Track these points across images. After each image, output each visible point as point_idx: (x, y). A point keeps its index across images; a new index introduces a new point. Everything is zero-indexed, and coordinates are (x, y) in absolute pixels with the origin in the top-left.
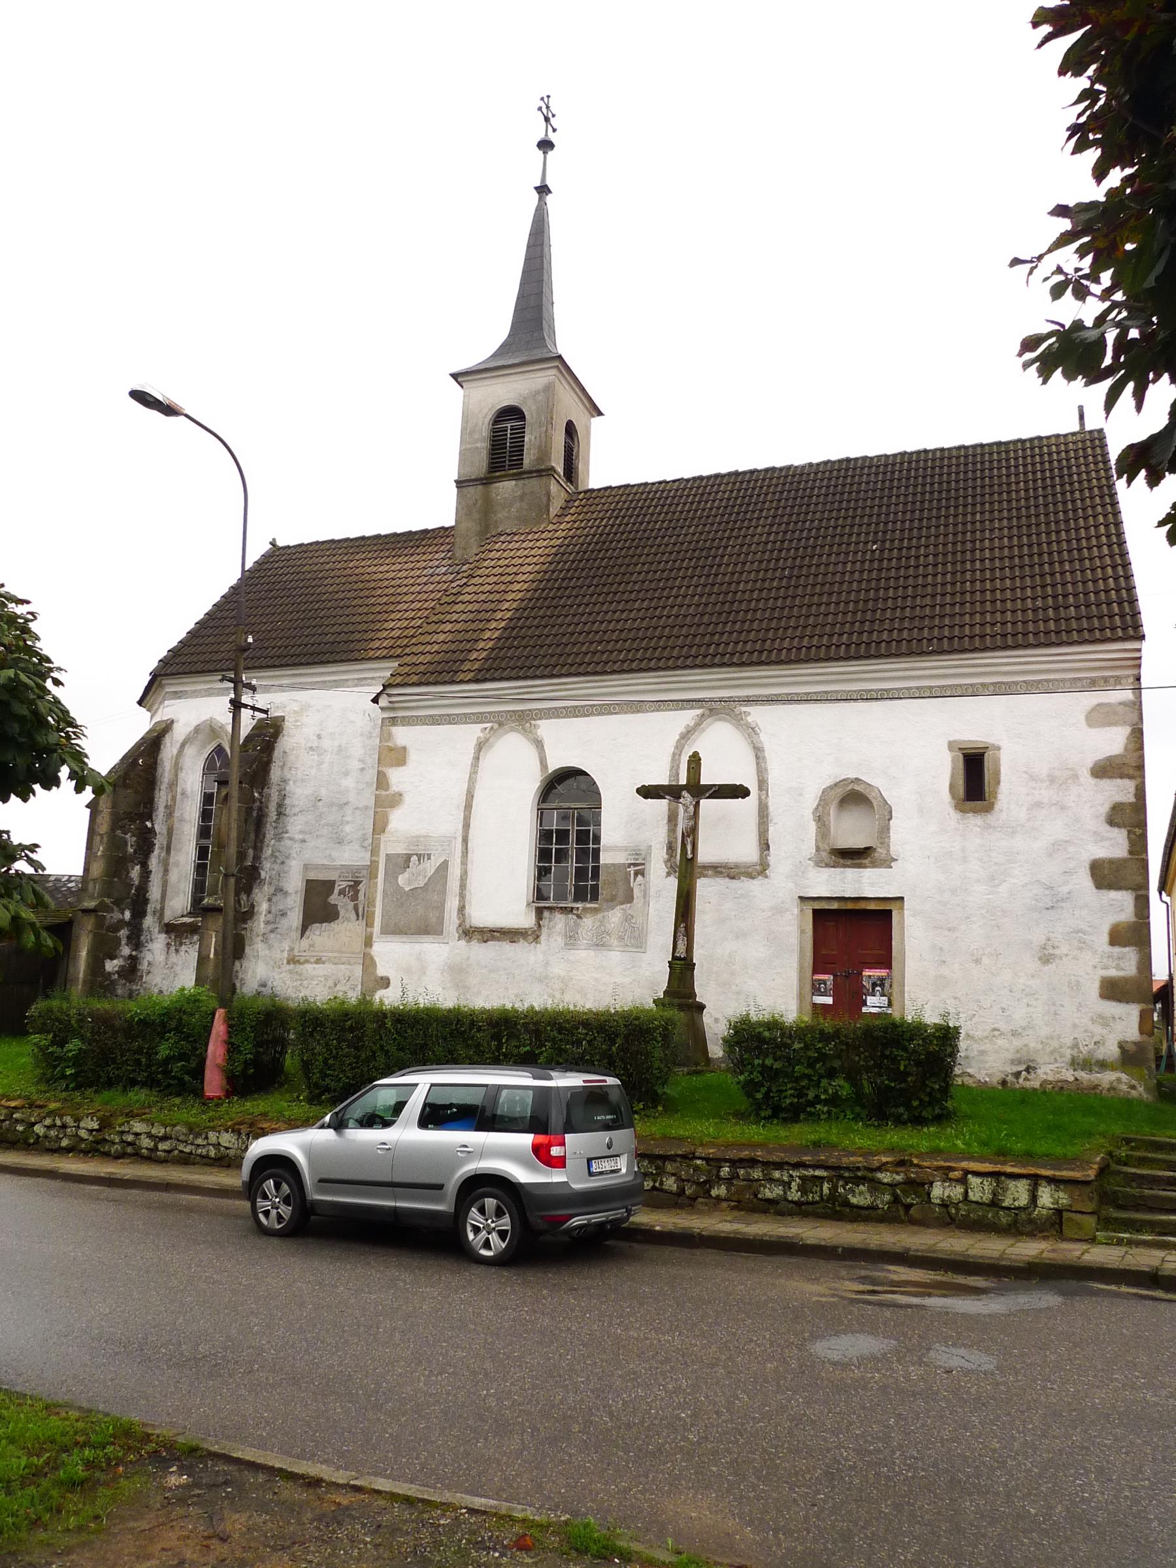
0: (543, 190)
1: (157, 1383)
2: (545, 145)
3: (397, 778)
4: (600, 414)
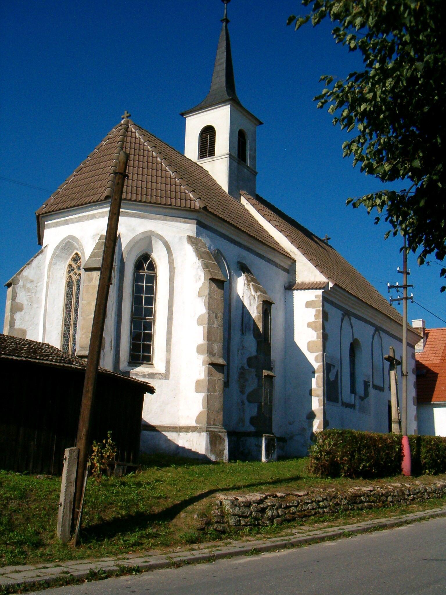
4: (261, 123)
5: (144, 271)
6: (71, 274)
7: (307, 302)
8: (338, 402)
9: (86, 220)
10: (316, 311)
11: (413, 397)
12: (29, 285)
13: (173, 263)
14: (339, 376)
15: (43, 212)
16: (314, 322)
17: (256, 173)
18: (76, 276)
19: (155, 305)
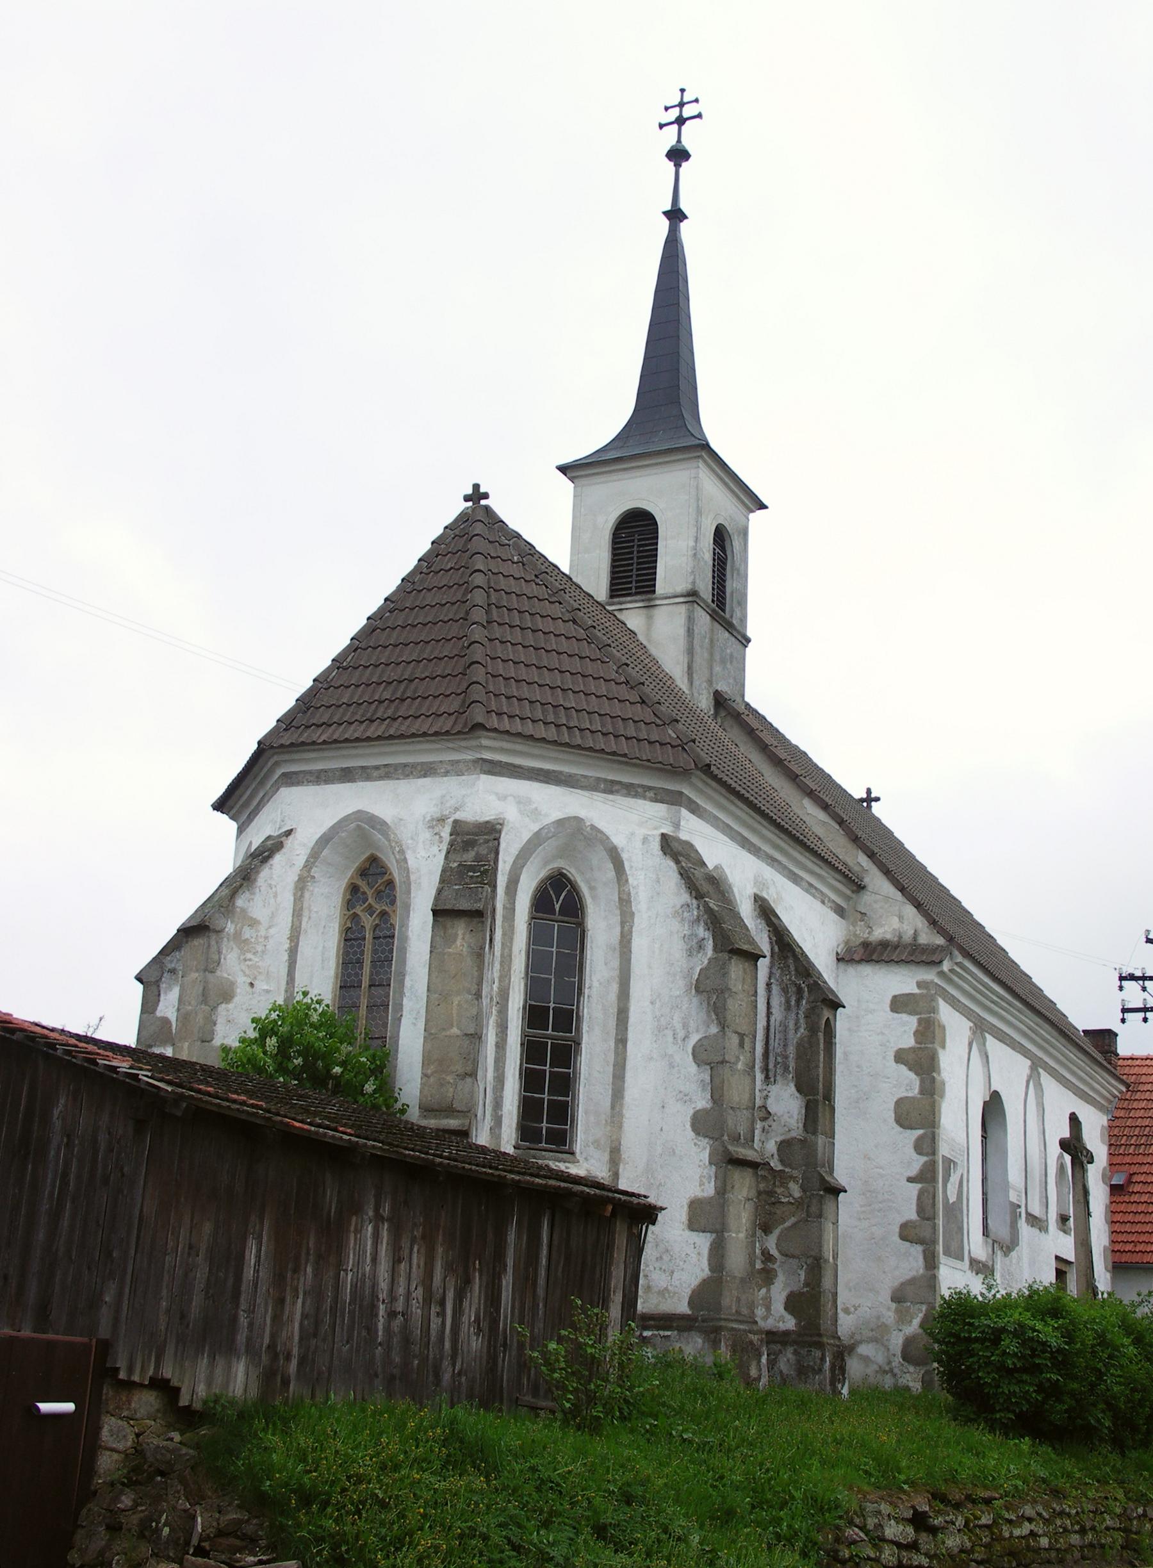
0: (675, 215)
1: (1061, 1530)
2: (678, 155)
3: (918, 1162)
4: (763, 506)
5: (552, 917)
6: (358, 910)
7: (895, 997)
8: (962, 1260)
9: (407, 776)
10: (920, 1021)
11: (1105, 1247)
12: (247, 933)
13: (629, 902)
14: (965, 1188)
15: (282, 741)
16: (912, 1050)
17: (748, 640)
18: (371, 919)
19: (578, 1002)
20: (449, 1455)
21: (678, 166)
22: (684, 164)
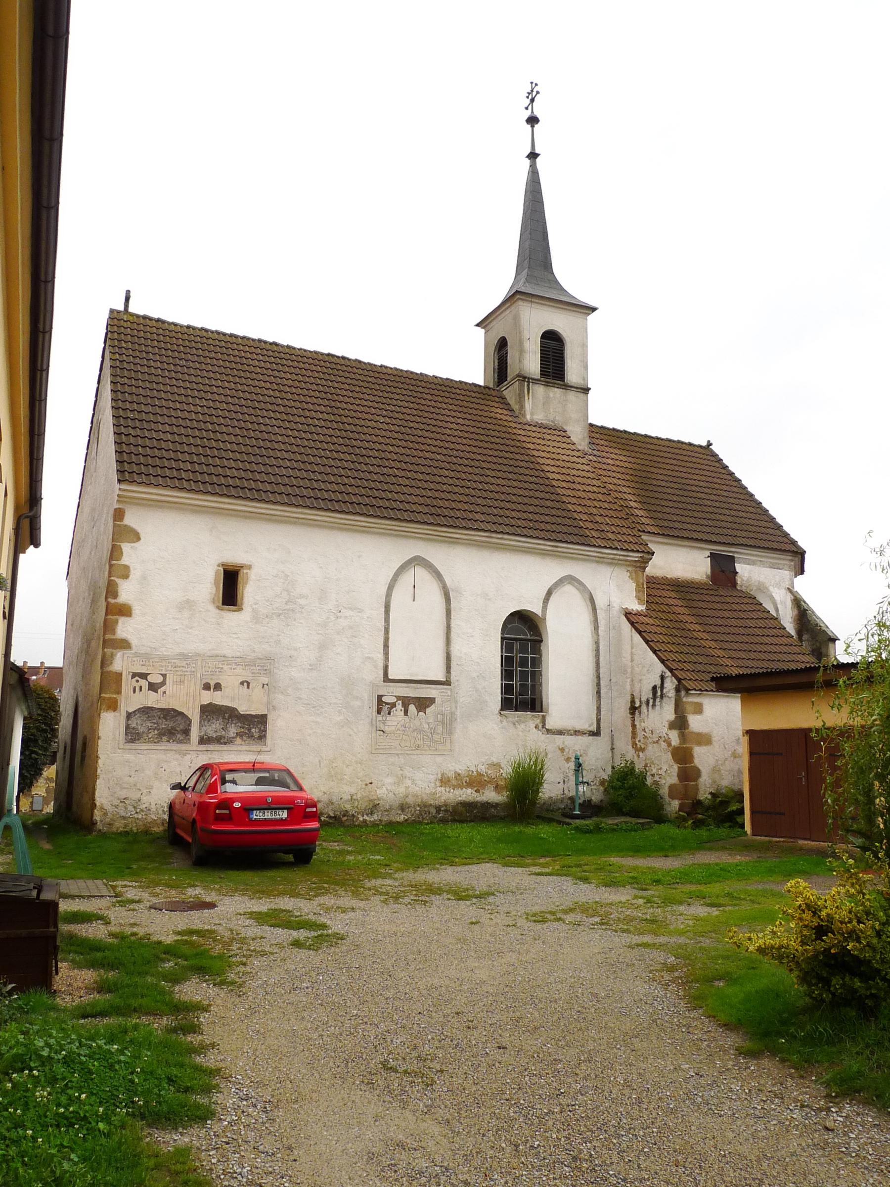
0: (533, 156)
4: (594, 309)
20: (93, 1151)
21: (533, 127)
22: (536, 126)
